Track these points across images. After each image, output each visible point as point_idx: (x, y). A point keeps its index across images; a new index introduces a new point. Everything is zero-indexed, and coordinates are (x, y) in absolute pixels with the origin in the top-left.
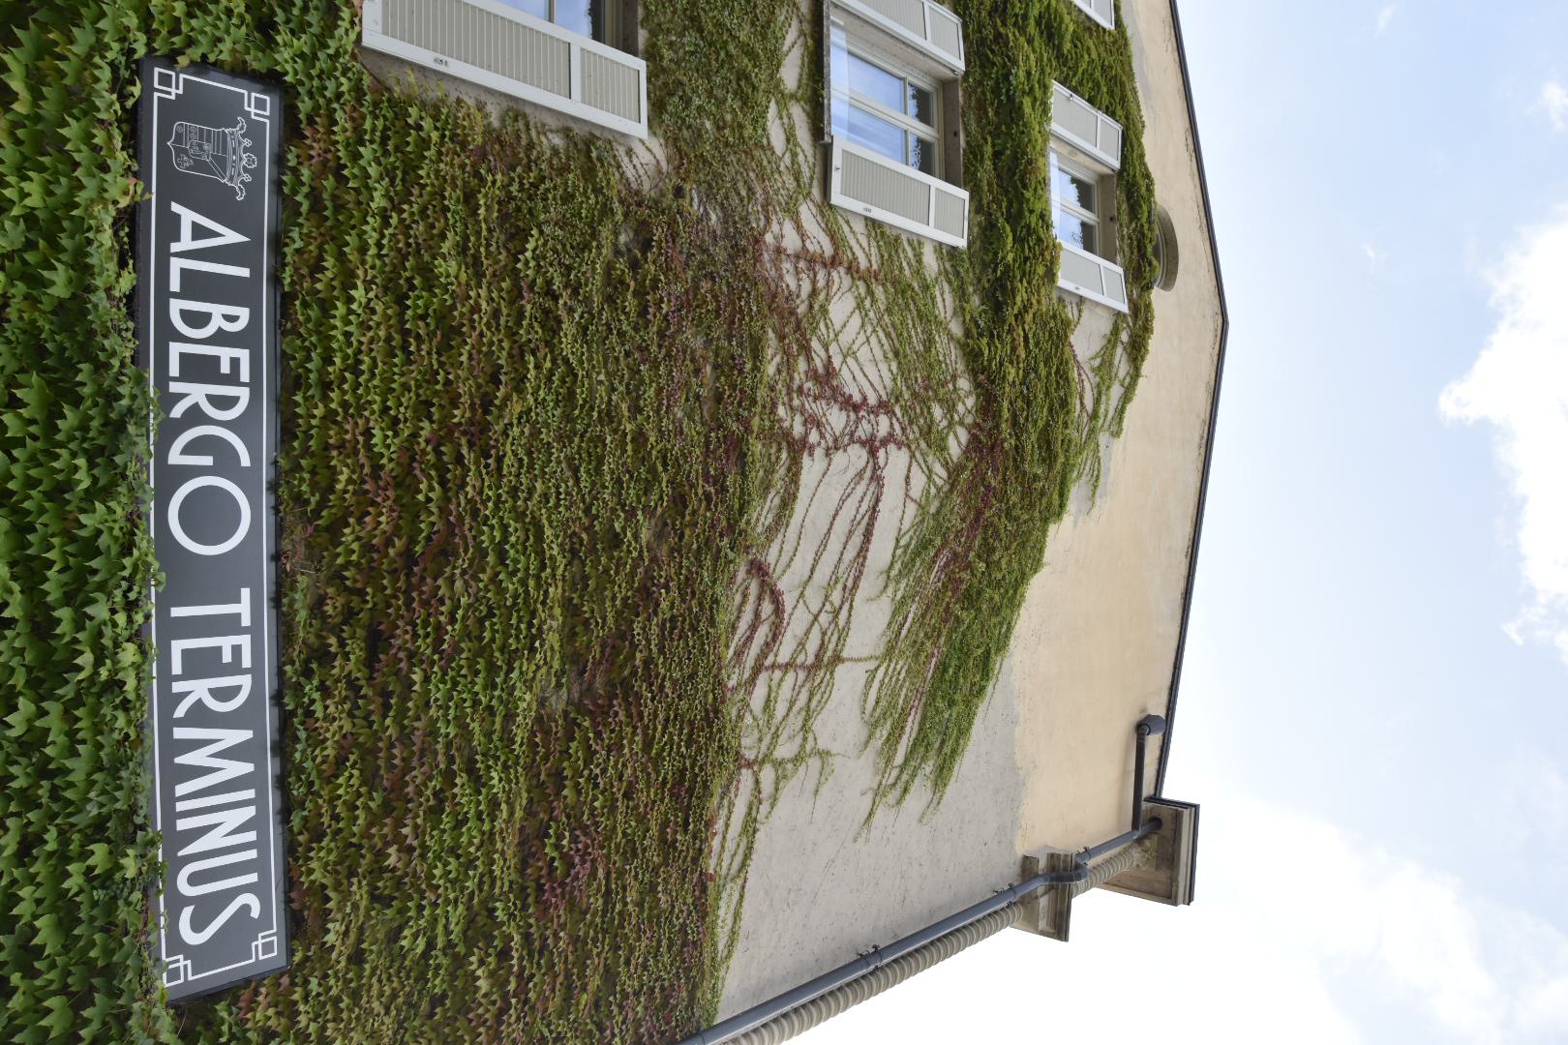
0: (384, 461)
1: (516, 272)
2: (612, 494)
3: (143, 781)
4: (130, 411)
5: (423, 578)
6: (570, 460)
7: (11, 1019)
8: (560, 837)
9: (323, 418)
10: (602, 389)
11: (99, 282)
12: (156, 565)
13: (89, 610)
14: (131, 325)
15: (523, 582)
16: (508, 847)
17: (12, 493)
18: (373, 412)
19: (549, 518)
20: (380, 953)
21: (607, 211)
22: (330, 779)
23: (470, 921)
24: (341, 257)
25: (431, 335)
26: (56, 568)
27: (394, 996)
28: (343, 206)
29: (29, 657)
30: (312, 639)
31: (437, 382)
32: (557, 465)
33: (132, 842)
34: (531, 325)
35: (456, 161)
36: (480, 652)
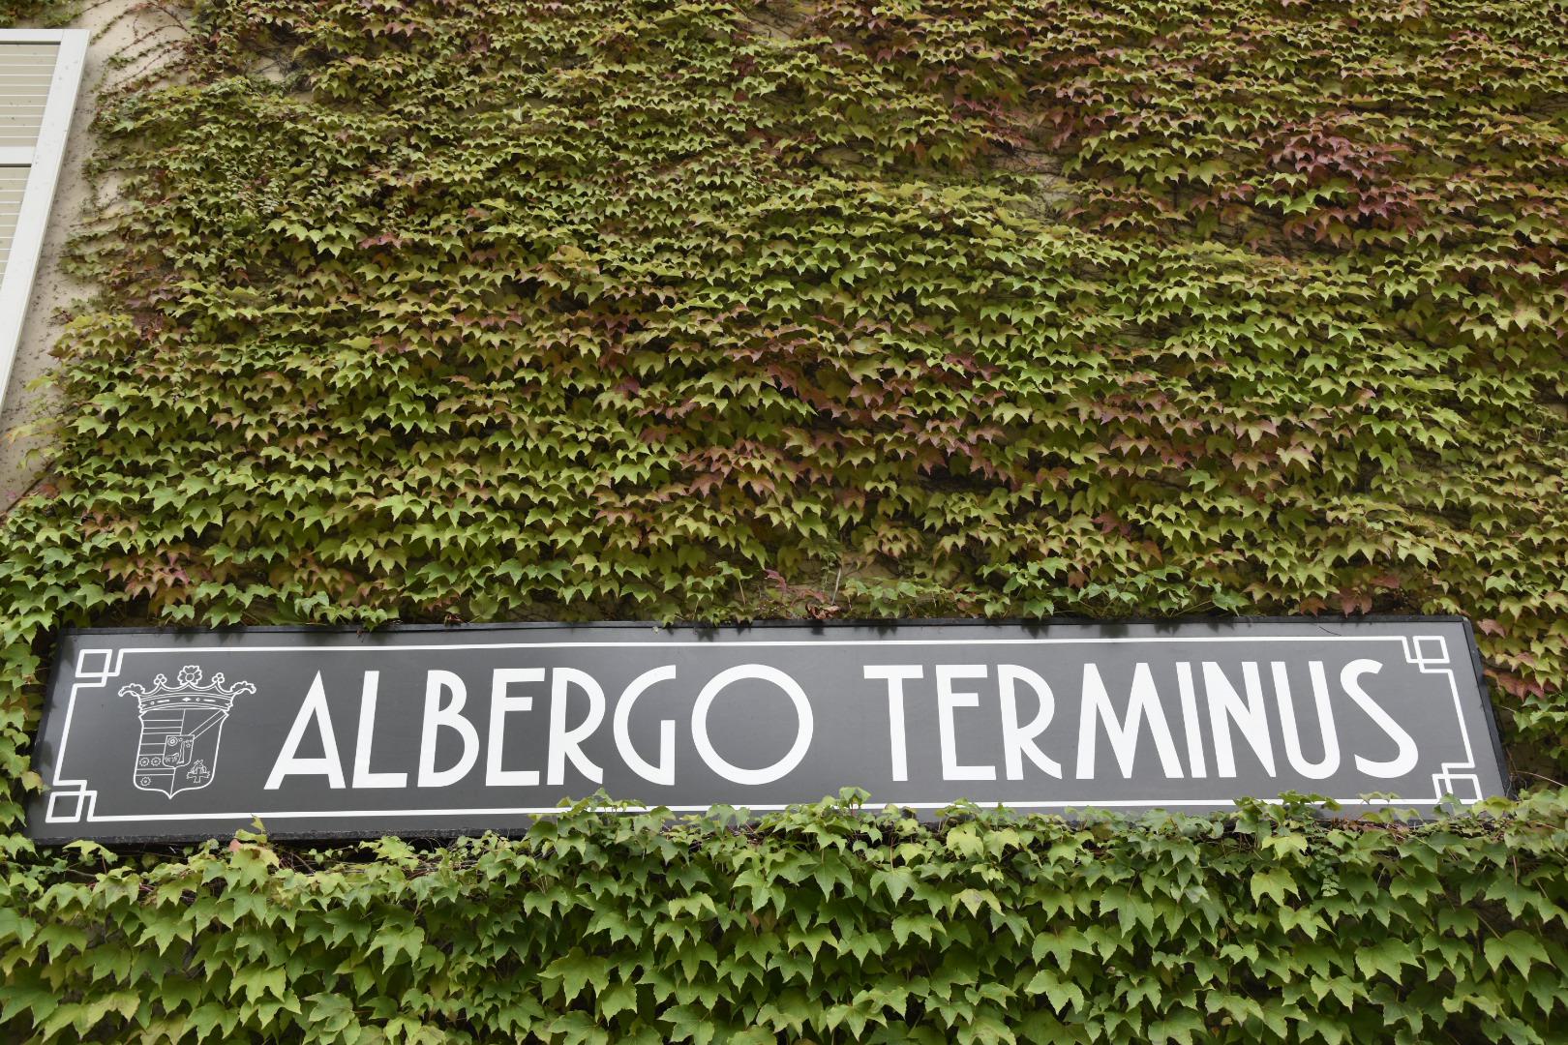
0: (664, 463)
1: (346, 258)
2: (713, 97)
3: (1157, 823)
4: (593, 840)
5: (851, 403)
6: (656, 168)
7: (1513, 1013)
8: (1282, 189)
9: (598, 556)
10: (539, 113)
11: (398, 888)
12: (829, 802)
13: (897, 895)
14: (462, 841)
15: (859, 244)
16: (1291, 274)
17: (721, 1001)
18: (587, 481)
19: (755, 202)
20: (1453, 480)
21: (227, 103)
22: (1166, 550)
23: (1412, 337)
24: (339, 533)
25: (459, 391)
26: (832, 941)
27: (1529, 460)
28: (256, 533)
29: (965, 979)
30: (944, 574)
31: (536, 381)
32: (667, 189)
33: (1251, 840)
34: (436, 232)
35: (165, 355)
36: (970, 315)
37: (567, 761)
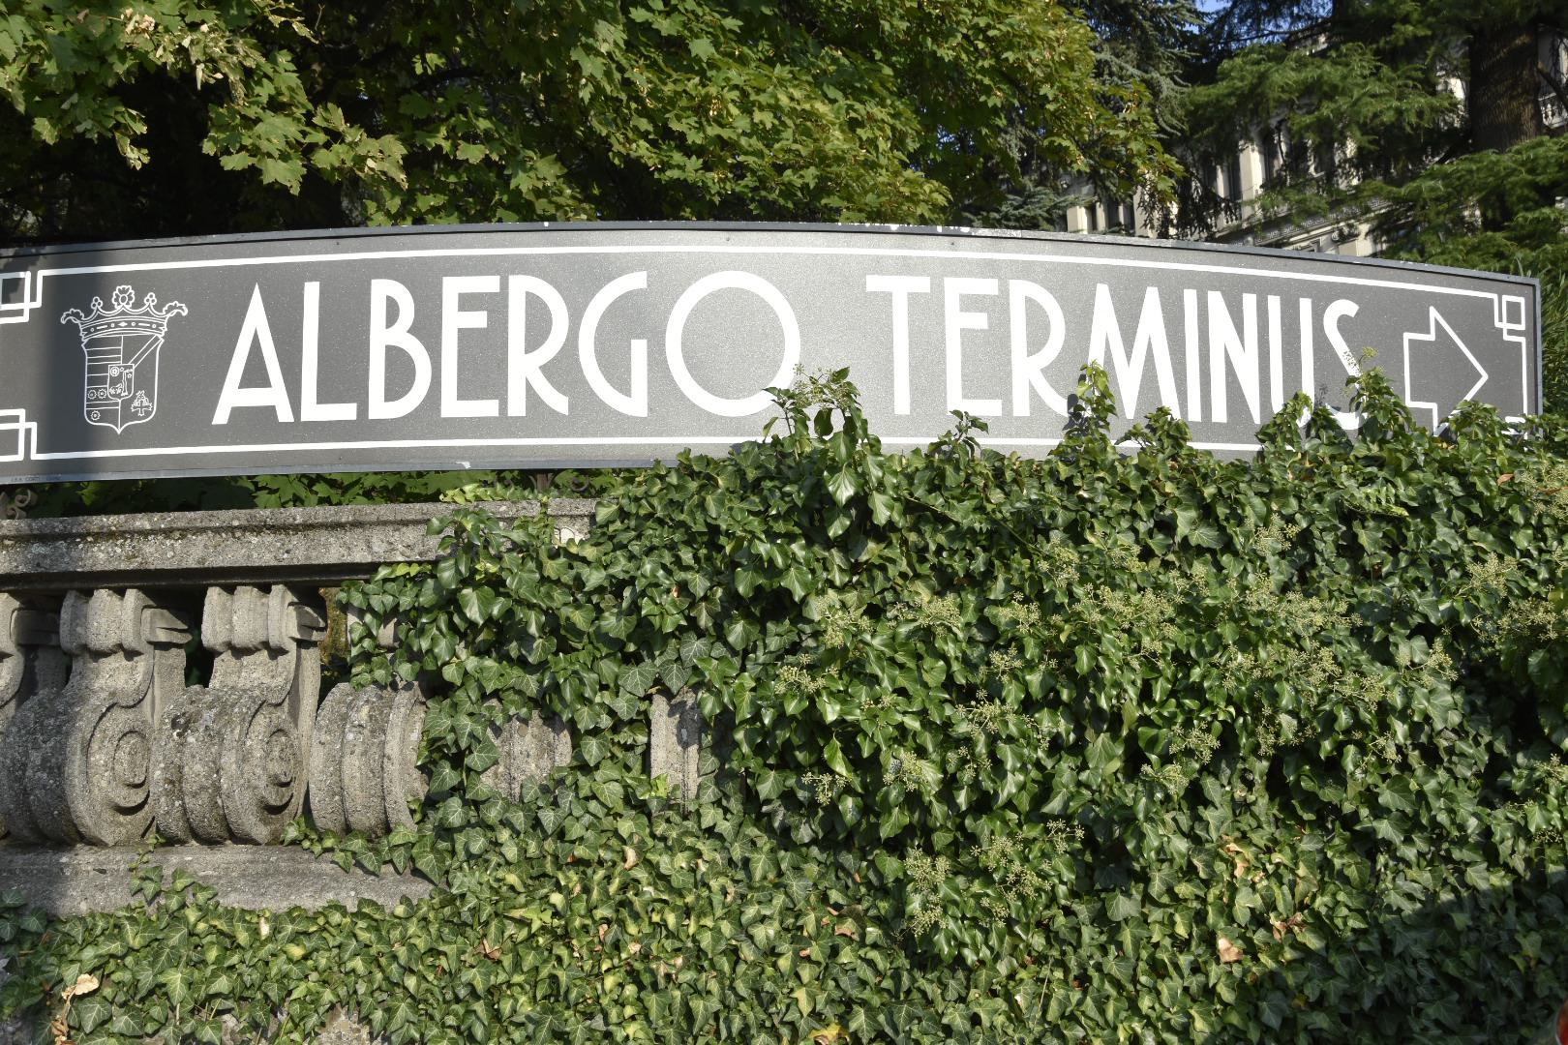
37: (529, 388)
